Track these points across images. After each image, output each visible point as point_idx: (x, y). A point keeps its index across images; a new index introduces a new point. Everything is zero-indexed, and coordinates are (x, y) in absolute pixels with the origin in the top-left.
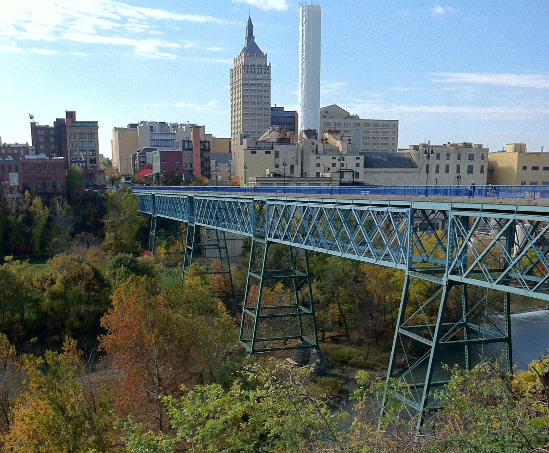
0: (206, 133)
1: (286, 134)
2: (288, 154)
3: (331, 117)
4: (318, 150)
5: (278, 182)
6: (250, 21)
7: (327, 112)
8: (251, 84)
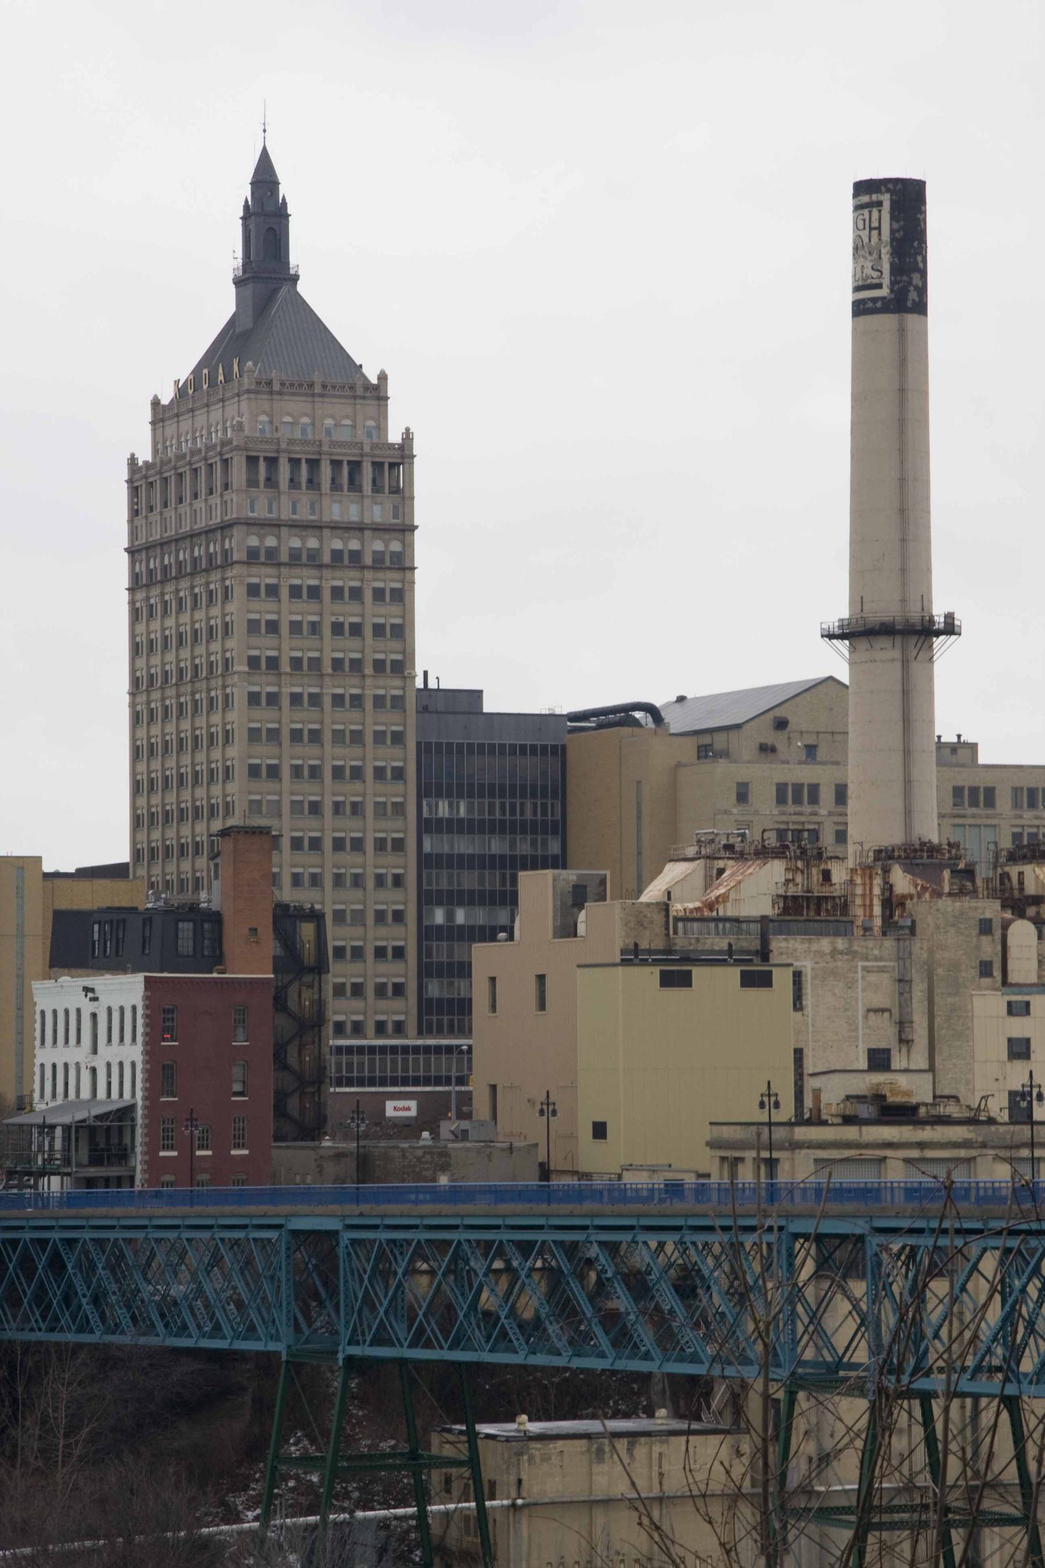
0: (522, 875)
1: (827, 875)
2: (850, 985)
3: (811, 750)
4: (1011, 966)
5: (915, 1154)
6: (265, 180)
7: (781, 724)
8: (337, 555)
